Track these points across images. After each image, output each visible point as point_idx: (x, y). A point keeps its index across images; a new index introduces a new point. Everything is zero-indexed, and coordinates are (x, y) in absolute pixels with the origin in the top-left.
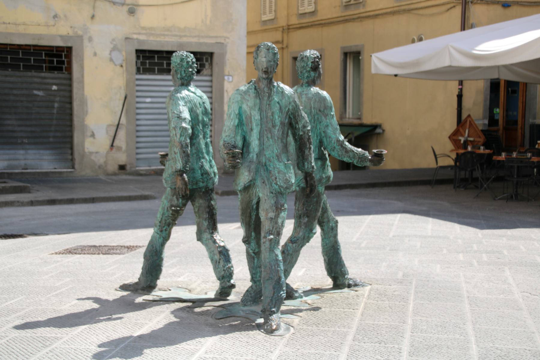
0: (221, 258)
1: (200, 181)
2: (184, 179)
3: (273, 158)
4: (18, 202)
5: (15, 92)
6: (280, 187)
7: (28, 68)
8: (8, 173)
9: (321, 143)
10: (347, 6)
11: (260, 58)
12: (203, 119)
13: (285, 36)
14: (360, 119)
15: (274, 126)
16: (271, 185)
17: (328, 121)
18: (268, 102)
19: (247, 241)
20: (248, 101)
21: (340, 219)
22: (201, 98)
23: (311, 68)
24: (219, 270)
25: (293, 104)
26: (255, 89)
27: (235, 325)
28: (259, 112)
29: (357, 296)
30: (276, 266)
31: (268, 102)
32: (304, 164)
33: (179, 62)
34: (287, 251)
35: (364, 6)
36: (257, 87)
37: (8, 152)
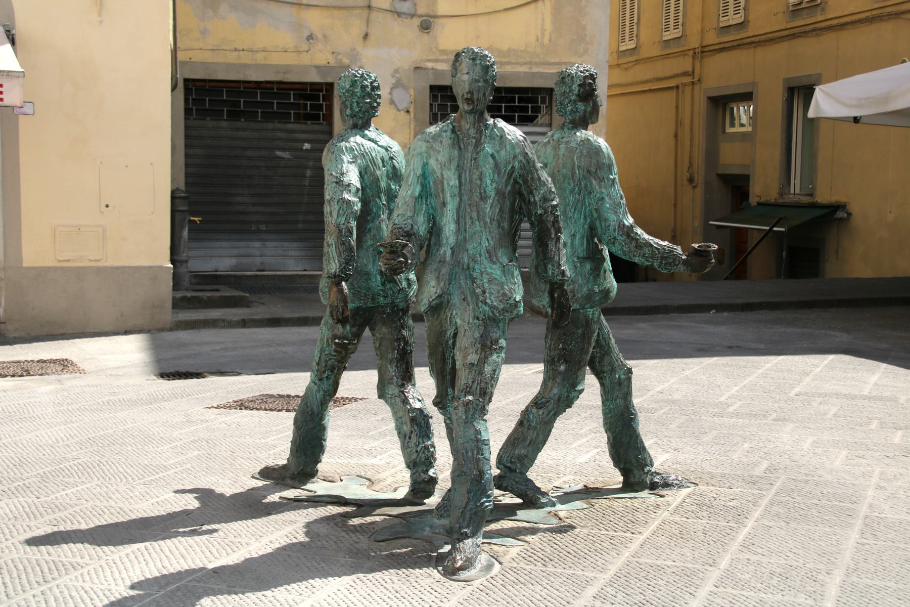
0: (414, 430)
1: (380, 295)
2: (341, 290)
3: (480, 255)
4: (223, 320)
5: (249, 153)
6: (492, 307)
7: (269, 116)
8: (234, 276)
9: (592, 232)
10: (796, 11)
11: (459, 75)
12: (389, 186)
13: (697, 64)
14: (811, 195)
15: (484, 198)
16: (477, 305)
17: (603, 190)
18: (474, 155)
19: (439, 403)
20: (439, 152)
21: (630, 363)
22: (387, 150)
23: (578, 95)
24: (409, 450)
25: (520, 158)
26: (453, 131)
27: (400, 554)
28: (457, 173)
29: (658, 506)
30: (475, 452)
31: (474, 155)
32: (546, 267)
33: (348, 87)
34: (528, 421)
35: (823, 10)
36: (457, 129)
37: (237, 244)
